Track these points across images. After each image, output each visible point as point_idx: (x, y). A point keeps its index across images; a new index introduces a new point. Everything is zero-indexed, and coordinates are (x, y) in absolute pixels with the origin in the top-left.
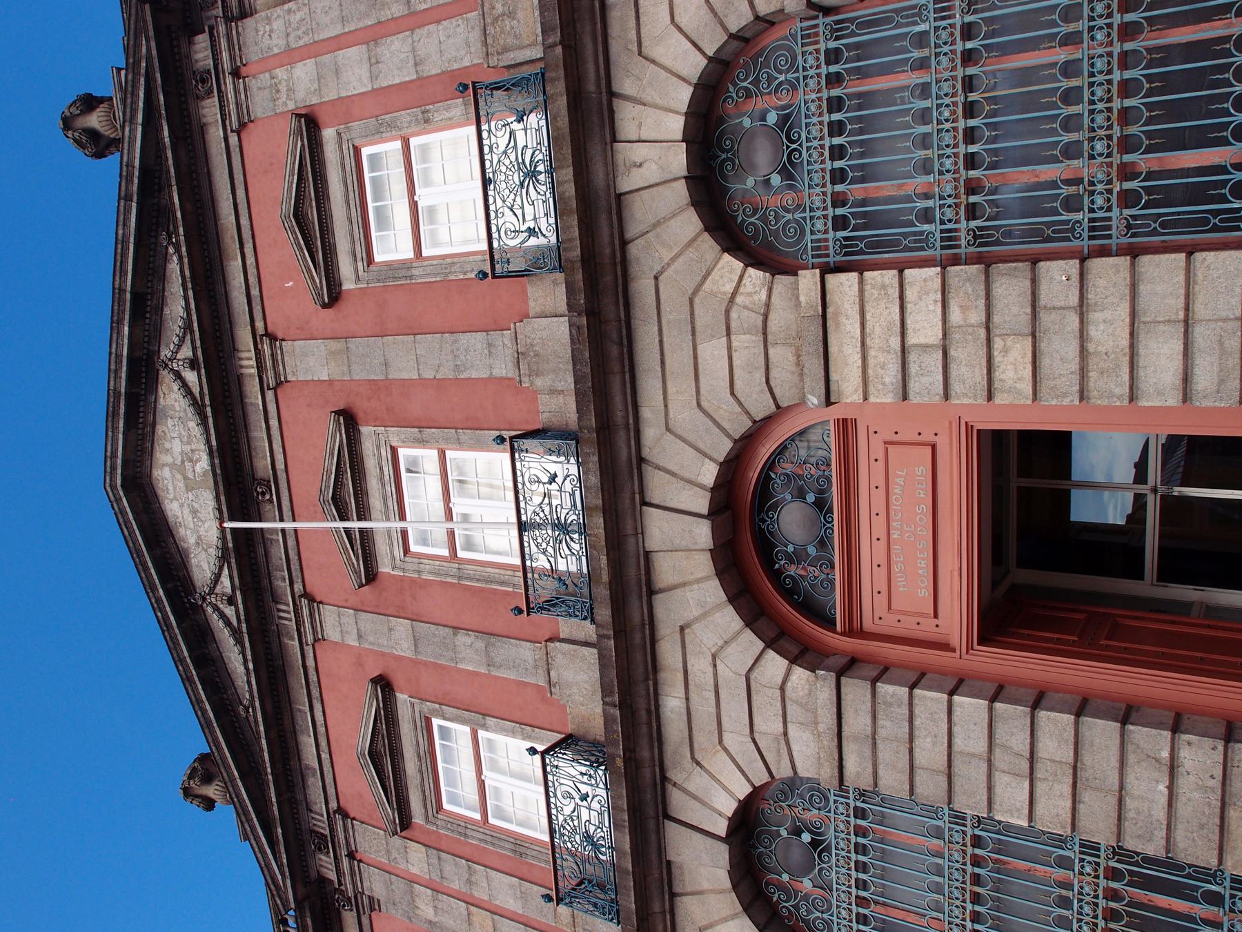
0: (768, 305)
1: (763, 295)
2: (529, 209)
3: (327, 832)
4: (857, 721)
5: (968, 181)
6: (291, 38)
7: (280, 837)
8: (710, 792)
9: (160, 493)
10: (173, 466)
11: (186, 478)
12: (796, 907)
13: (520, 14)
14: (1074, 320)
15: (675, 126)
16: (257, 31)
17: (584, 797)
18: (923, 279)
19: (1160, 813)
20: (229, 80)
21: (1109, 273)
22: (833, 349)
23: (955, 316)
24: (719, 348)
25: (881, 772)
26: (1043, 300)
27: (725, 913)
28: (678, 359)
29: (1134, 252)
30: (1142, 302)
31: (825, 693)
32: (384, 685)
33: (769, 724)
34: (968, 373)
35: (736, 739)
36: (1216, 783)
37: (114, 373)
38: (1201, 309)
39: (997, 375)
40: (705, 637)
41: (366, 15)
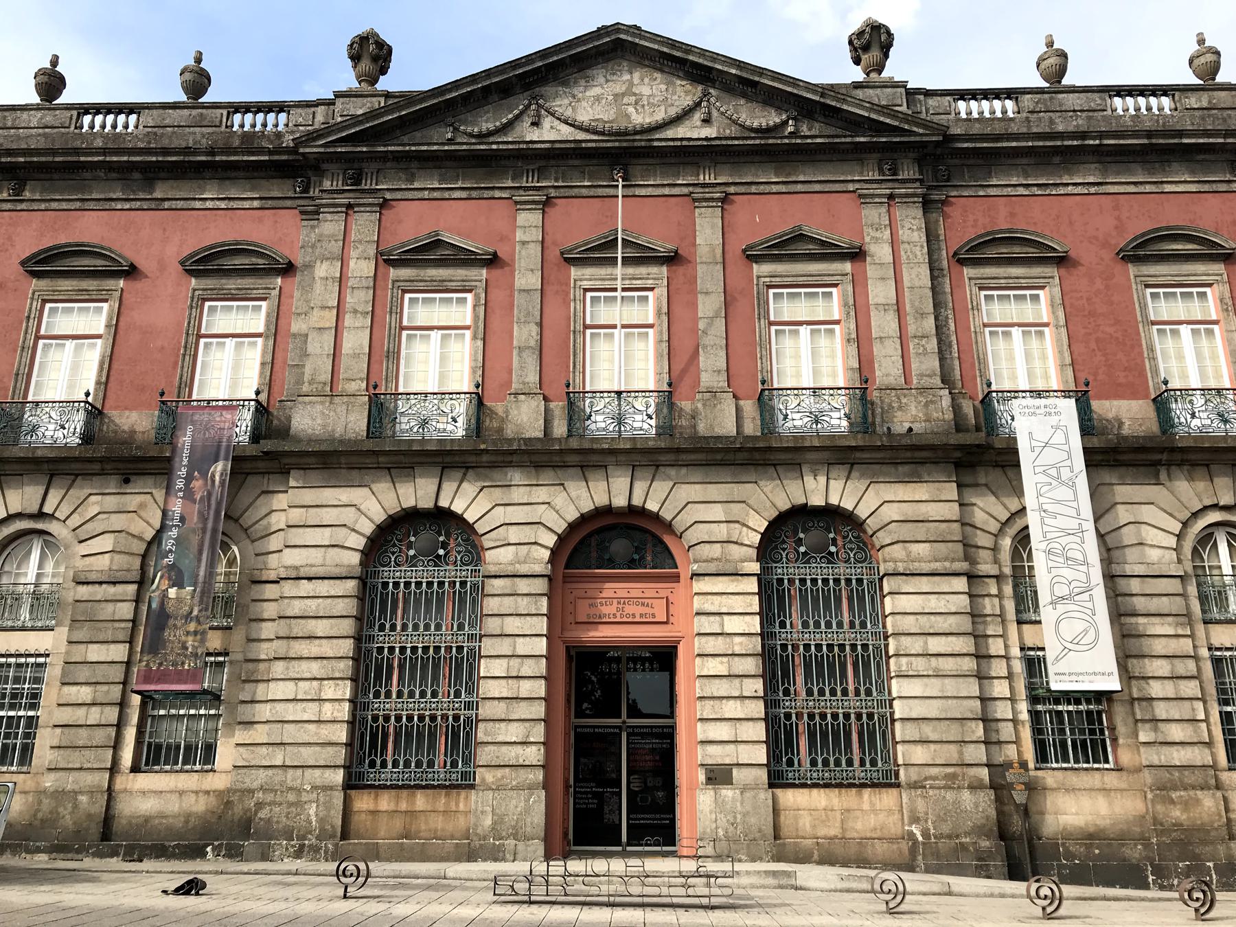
0: (742, 544)
1: (747, 542)
3: (363, 187)
4: (523, 586)
5: (798, 646)
6: (906, 246)
7: (359, 149)
8: (466, 499)
9: (610, 65)
10: (631, 84)
11: (623, 95)
12: (394, 545)
15: (834, 500)
16: (914, 218)
17: (455, 420)
18: (754, 624)
19: (500, 739)
20: (888, 191)
21: (758, 709)
22: (720, 578)
23: (737, 639)
24: (720, 520)
25: (496, 598)
26: (746, 680)
27: (386, 505)
28: (714, 492)
30: (745, 723)
31: (538, 569)
32: (492, 261)
33: (514, 534)
34: (712, 645)
35: (500, 515)
36: (521, 762)
37: (703, 52)
38: (741, 747)
39: (710, 659)
40: (560, 499)
41: (912, 306)
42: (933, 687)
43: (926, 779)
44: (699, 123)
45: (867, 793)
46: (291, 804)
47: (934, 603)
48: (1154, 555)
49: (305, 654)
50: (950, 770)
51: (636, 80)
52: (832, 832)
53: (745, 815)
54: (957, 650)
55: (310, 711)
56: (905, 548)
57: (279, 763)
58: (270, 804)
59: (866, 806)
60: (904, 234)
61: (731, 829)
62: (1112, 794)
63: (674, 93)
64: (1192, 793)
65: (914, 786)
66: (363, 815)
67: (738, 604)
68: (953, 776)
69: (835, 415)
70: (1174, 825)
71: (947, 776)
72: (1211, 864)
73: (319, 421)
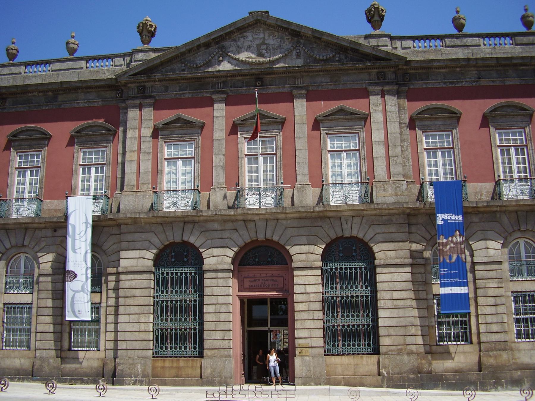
1: (317, 253)
2: (338, 196)
13: (384, 193)
14: (311, 318)
15: (354, 234)
16: (393, 100)
19: (213, 338)
23: (312, 295)
29: (324, 328)
36: (222, 347)
37: (297, 25)
42: (395, 313)
43: (389, 351)
44: (295, 57)
45: (365, 357)
46: (131, 364)
47: (396, 277)
48: (492, 252)
49: (132, 303)
50: (399, 347)
51: (266, 37)
52: (350, 373)
53: (314, 367)
54: (405, 297)
55: (136, 327)
56: (385, 253)
57: (124, 348)
58: (122, 364)
59: (364, 363)
60: (388, 108)
61: (308, 373)
62: (467, 354)
63: (284, 43)
64: (498, 352)
65: (386, 354)
66: (159, 369)
67: (312, 280)
68: (401, 349)
69: (355, 195)
70: (490, 365)
71: (398, 350)
72: (503, 381)
73: (131, 203)
